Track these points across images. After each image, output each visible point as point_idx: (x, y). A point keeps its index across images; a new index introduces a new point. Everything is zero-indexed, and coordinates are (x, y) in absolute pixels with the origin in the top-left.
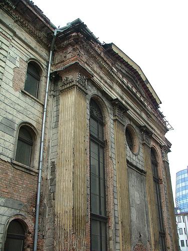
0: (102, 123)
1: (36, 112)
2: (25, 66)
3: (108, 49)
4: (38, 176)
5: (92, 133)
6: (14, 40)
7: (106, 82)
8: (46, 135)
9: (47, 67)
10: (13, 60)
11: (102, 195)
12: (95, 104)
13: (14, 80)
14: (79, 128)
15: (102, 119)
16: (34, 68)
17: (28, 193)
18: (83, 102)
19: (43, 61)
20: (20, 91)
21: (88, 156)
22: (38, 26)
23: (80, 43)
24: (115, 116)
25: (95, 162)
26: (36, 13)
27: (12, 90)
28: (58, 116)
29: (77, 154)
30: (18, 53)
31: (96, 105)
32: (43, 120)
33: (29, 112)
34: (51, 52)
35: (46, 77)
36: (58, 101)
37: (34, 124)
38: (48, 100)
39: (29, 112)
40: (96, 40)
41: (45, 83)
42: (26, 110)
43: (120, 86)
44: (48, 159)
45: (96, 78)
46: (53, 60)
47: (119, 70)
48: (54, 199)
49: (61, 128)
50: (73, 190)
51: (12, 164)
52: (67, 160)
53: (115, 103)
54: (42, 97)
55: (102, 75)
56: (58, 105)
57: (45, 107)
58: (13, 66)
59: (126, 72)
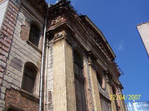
33: (32, 56)
37: (36, 64)
51: (20, 92)
57: (43, 53)
58: (21, 24)
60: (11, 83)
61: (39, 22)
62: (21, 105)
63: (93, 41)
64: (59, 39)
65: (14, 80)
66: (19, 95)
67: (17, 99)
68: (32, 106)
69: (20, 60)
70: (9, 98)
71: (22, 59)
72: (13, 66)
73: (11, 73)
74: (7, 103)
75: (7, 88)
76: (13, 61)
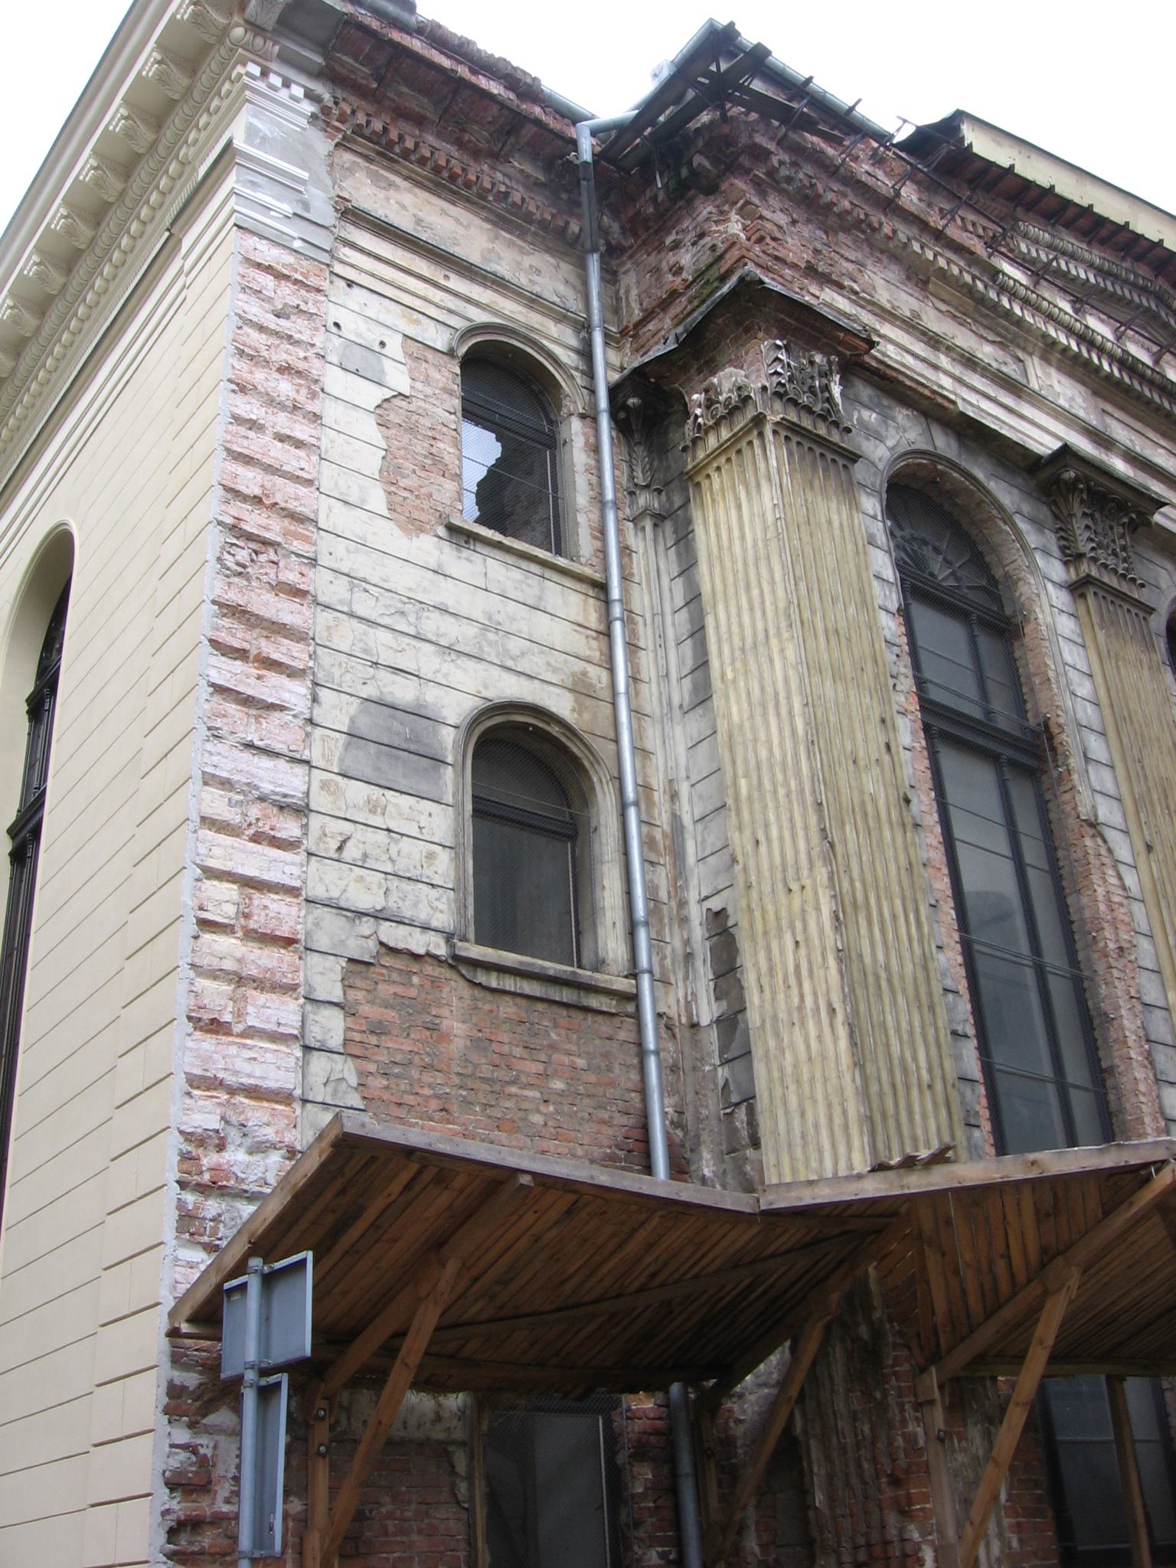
0: (997, 622)
1: (559, 634)
2: (448, 375)
3: (942, 154)
4: (637, 1016)
5: (935, 694)
6: (353, 246)
7: (970, 362)
8: (649, 759)
9: (586, 353)
10: (363, 363)
11: (1076, 1072)
12: (922, 502)
13: (390, 475)
14: (837, 676)
15: (997, 599)
16: (500, 378)
17: (588, 1128)
18: (831, 510)
19: (553, 329)
20: (442, 531)
21: (933, 836)
22: (478, 135)
23: (744, 160)
24: (1071, 557)
25: (989, 874)
26: (446, 63)
27: (389, 535)
28: (698, 632)
29: (851, 838)
30: (392, 315)
31: (940, 520)
32: (611, 670)
33: (514, 645)
34: (594, 263)
35: (590, 417)
36: (684, 540)
37: (561, 704)
38: (625, 551)
39: (514, 645)
40: (844, 124)
41: (590, 459)
42: (499, 632)
43: (1077, 368)
44: (682, 904)
45: (897, 349)
46: (614, 307)
47: (1039, 272)
48: (756, 1143)
49: (731, 707)
50: (859, 1064)
51: (457, 962)
52: (795, 887)
53: (1058, 480)
54: (586, 544)
55: (934, 321)
56: (688, 567)
57: (615, 593)
58: (373, 395)
59: (1100, 271)
60: (378, 916)
61: (535, 319)
62: (486, 1071)
63: (1085, 338)
64: (725, 434)
65: (394, 883)
66: (455, 993)
67: (445, 1024)
68: (581, 1062)
69: (417, 713)
70: (378, 1029)
71: (432, 695)
72: (369, 773)
73: (359, 833)
74: (372, 1068)
75: (350, 960)
76: (365, 733)
